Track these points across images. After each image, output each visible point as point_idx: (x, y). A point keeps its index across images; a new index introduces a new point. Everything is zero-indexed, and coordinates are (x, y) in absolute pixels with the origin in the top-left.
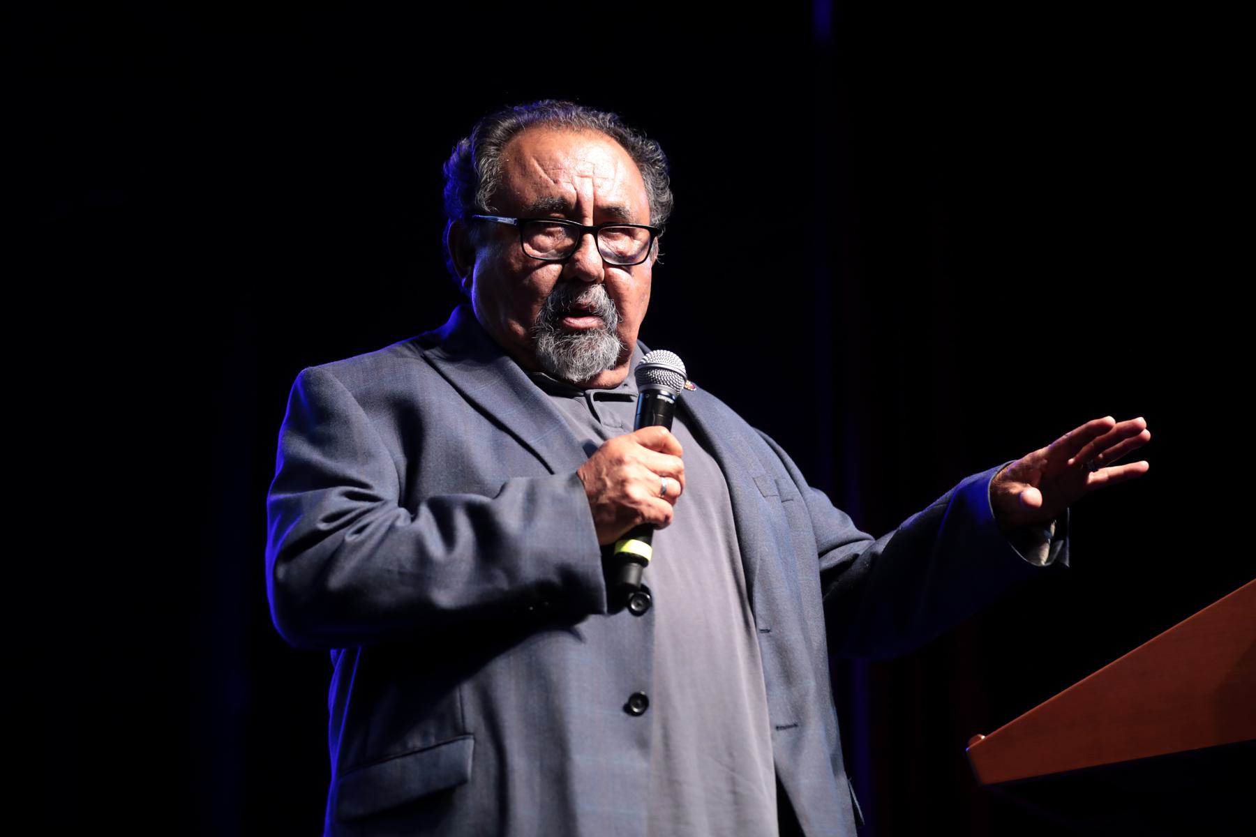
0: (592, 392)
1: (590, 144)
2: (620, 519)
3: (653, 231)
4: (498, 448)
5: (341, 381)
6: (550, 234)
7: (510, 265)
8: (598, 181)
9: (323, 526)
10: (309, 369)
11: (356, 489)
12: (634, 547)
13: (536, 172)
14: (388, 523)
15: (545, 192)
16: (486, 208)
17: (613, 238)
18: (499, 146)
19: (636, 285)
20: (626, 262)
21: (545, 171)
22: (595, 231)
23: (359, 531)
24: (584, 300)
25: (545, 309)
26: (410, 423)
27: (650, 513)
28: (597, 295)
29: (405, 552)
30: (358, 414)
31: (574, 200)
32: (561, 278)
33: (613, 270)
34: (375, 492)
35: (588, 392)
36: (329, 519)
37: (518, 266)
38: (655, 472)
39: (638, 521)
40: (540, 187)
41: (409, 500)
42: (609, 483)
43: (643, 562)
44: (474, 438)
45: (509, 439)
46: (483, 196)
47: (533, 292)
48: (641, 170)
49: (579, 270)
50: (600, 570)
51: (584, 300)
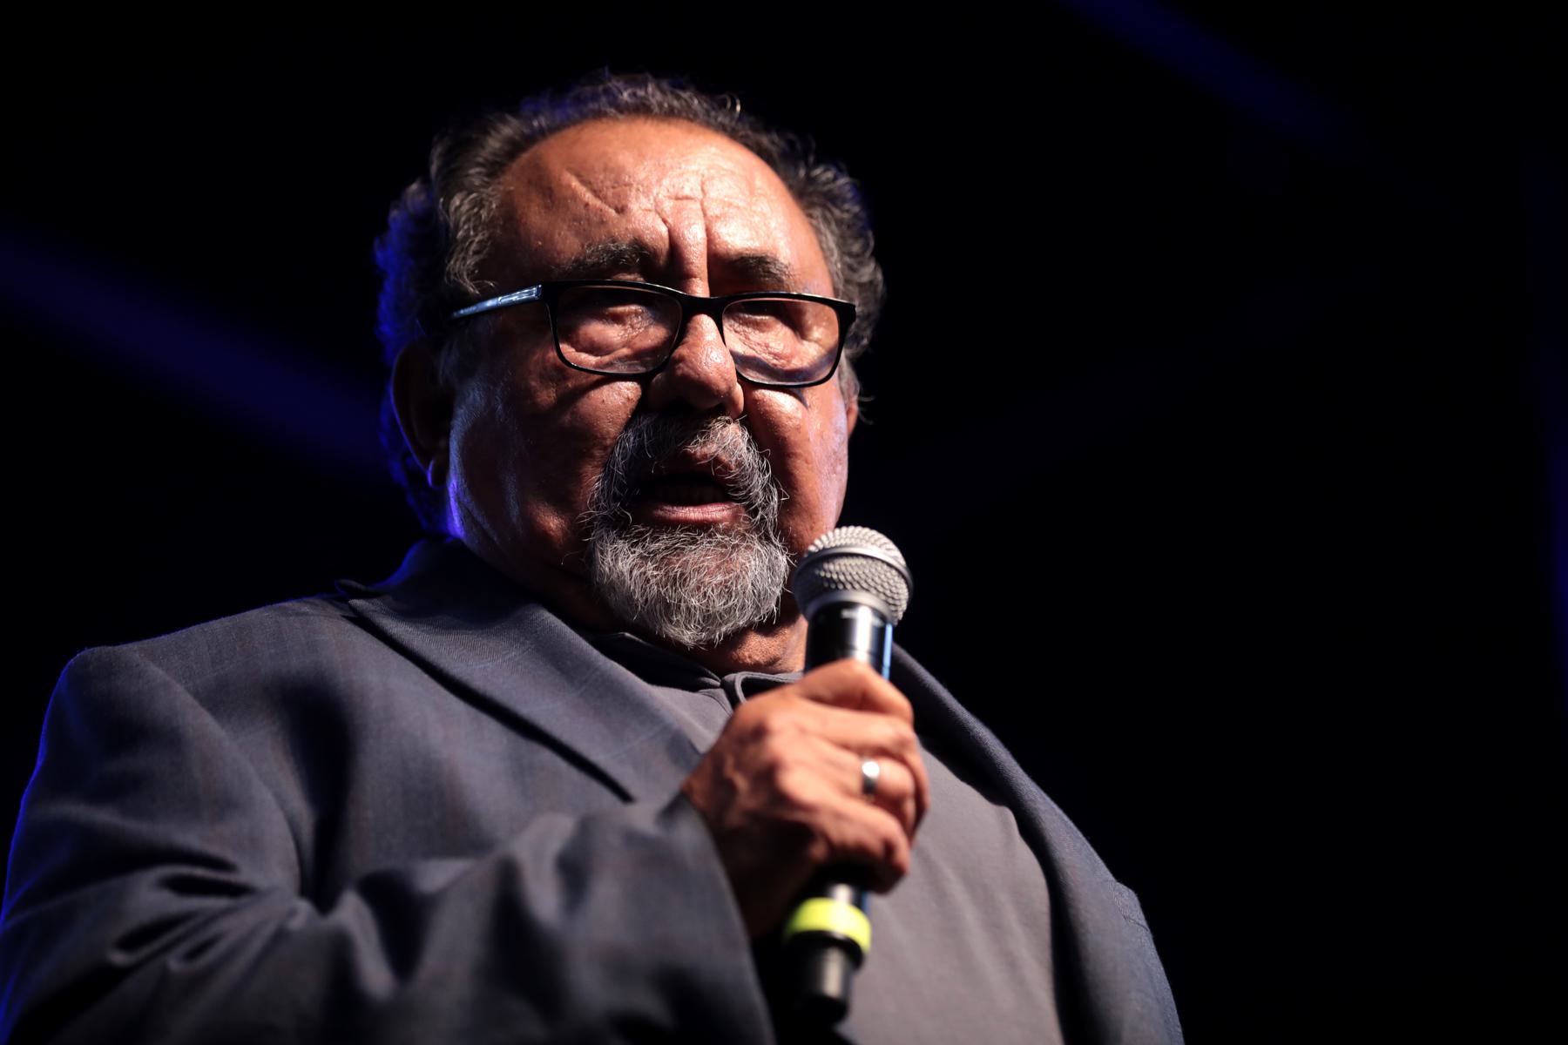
0: (738, 678)
1: (691, 140)
2: (777, 853)
3: (845, 313)
4: (521, 772)
5: (165, 672)
6: (618, 319)
7: (529, 394)
8: (714, 210)
9: (119, 958)
10: (87, 652)
11: (199, 872)
12: (835, 913)
13: (575, 196)
14: (269, 930)
15: (600, 234)
16: (471, 289)
17: (757, 326)
18: (495, 169)
19: (822, 424)
20: (795, 382)
21: (596, 193)
22: (718, 309)
23: (193, 955)
24: (703, 449)
25: (609, 475)
26: (322, 731)
27: (847, 833)
28: (729, 441)
29: (308, 986)
30: (200, 723)
31: (664, 246)
32: (642, 408)
33: (761, 394)
34: (246, 874)
35: (729, 677)
36: (130, 942)
37: (547, 396)
38: (846, 746)
39: (818, 851)
40: (586, 222)
41: (320, 884)
42: (741, 782)
43: (850, 949)
44: (473, 755)
45: (547, 756)
46: (462, 266)
47: (582, 439)
48: (810, 216)
49: (686, 379)
50: (750, 977)
51: (703, 449)
